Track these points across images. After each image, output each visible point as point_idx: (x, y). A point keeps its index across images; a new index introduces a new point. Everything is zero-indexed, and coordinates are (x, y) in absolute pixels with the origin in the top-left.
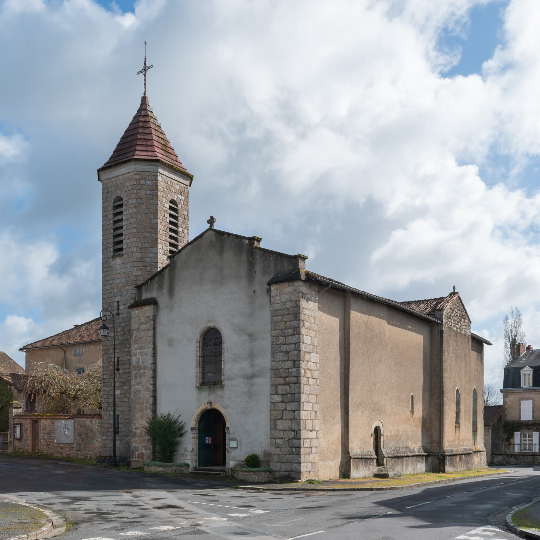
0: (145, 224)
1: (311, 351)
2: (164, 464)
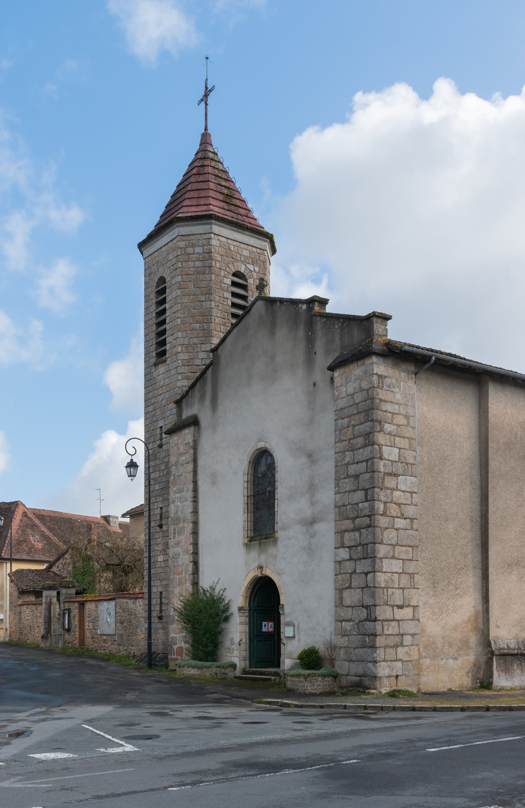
0: (193, 311)
1: (400, 472)
2: (200, 663)
